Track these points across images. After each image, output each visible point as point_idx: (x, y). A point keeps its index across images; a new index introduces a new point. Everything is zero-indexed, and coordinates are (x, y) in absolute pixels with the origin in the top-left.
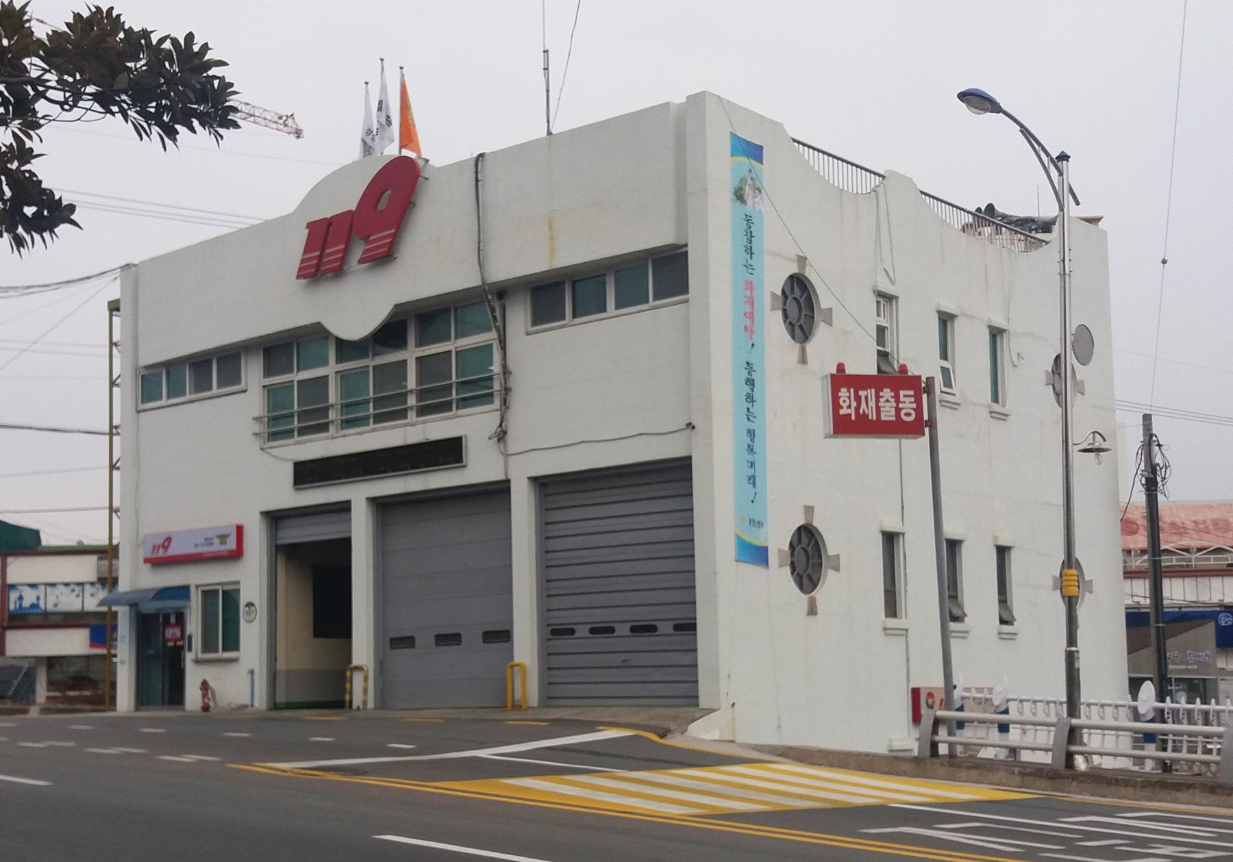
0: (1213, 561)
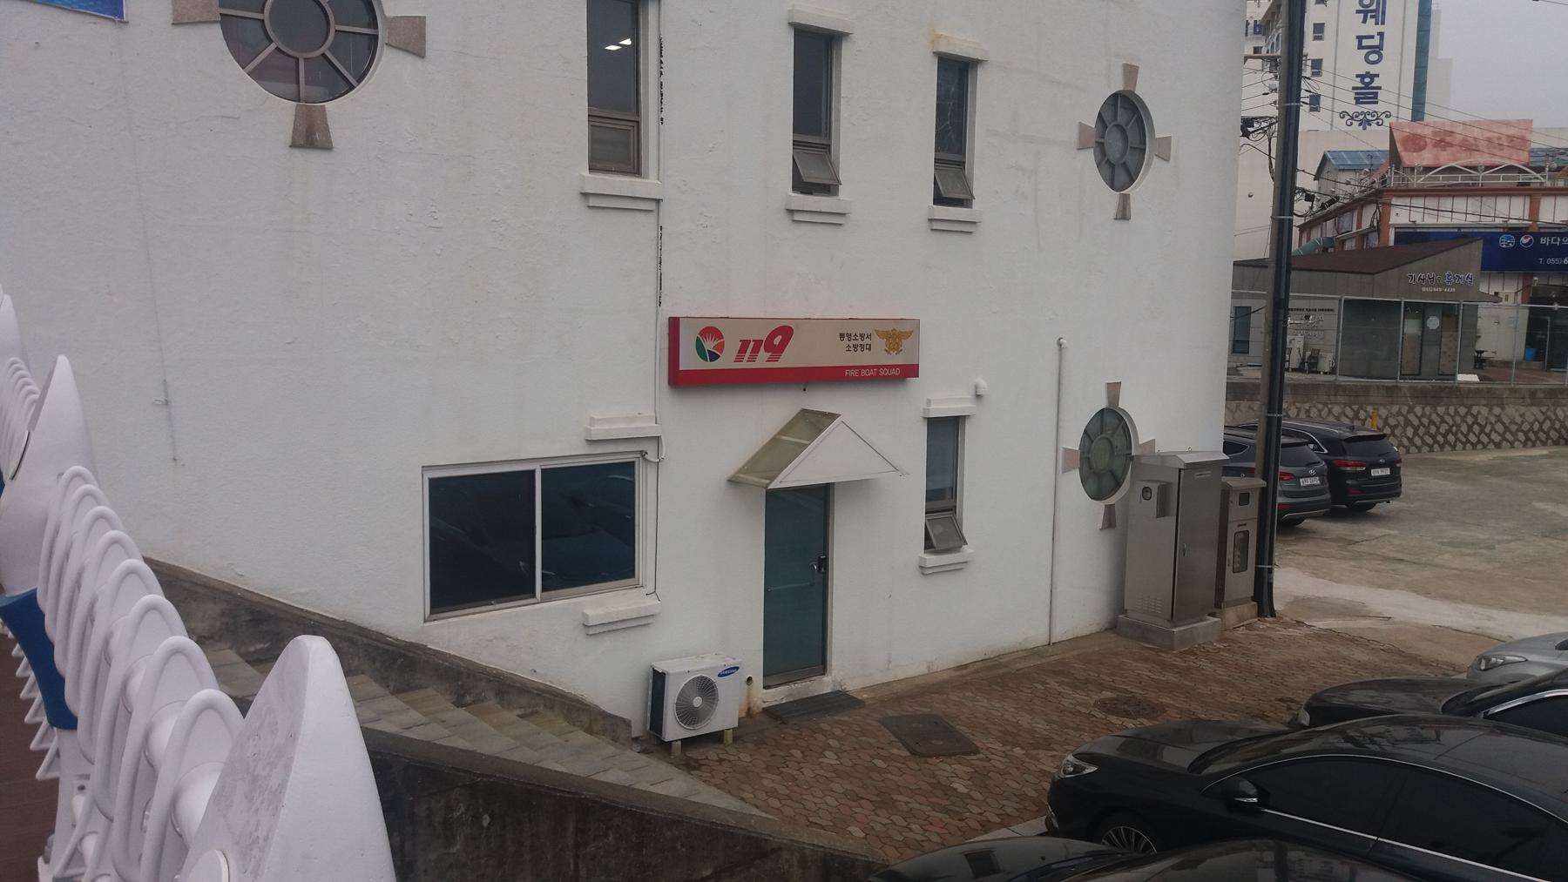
0: (1502, 180)
